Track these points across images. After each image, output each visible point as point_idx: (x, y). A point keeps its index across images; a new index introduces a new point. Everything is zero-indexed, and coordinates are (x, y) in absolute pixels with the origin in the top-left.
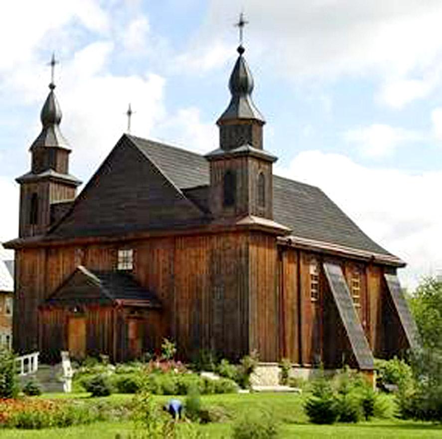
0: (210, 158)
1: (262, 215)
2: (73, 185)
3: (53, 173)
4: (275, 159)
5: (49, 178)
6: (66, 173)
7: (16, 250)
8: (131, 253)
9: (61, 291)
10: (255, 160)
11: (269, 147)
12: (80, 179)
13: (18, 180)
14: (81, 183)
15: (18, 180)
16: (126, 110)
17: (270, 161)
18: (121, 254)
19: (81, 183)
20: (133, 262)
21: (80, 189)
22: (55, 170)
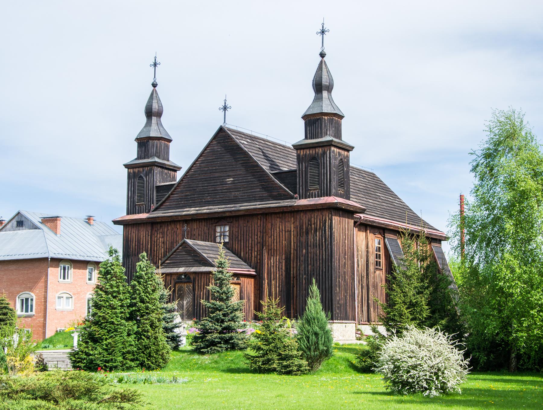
0: (297, 147)
1: (341, 196)
2: (175, 169)
3: (157, 160)
4: (181, 168)
5: (154, 164)
6: (168, 160)
7: (124, 225)
8: (227, 228)
9: (172, 256)
10: (376, 230)
11: (346, 138)
12: (178, 164)
13: (126, 166)
14: (180, 168)
15: (126, 166)
16: (222, 105)
17: (348, 149)
18: (218, 229)
19: (180, 168)
20: (229, 236)
21: (179, 175)
22: (159, 157)
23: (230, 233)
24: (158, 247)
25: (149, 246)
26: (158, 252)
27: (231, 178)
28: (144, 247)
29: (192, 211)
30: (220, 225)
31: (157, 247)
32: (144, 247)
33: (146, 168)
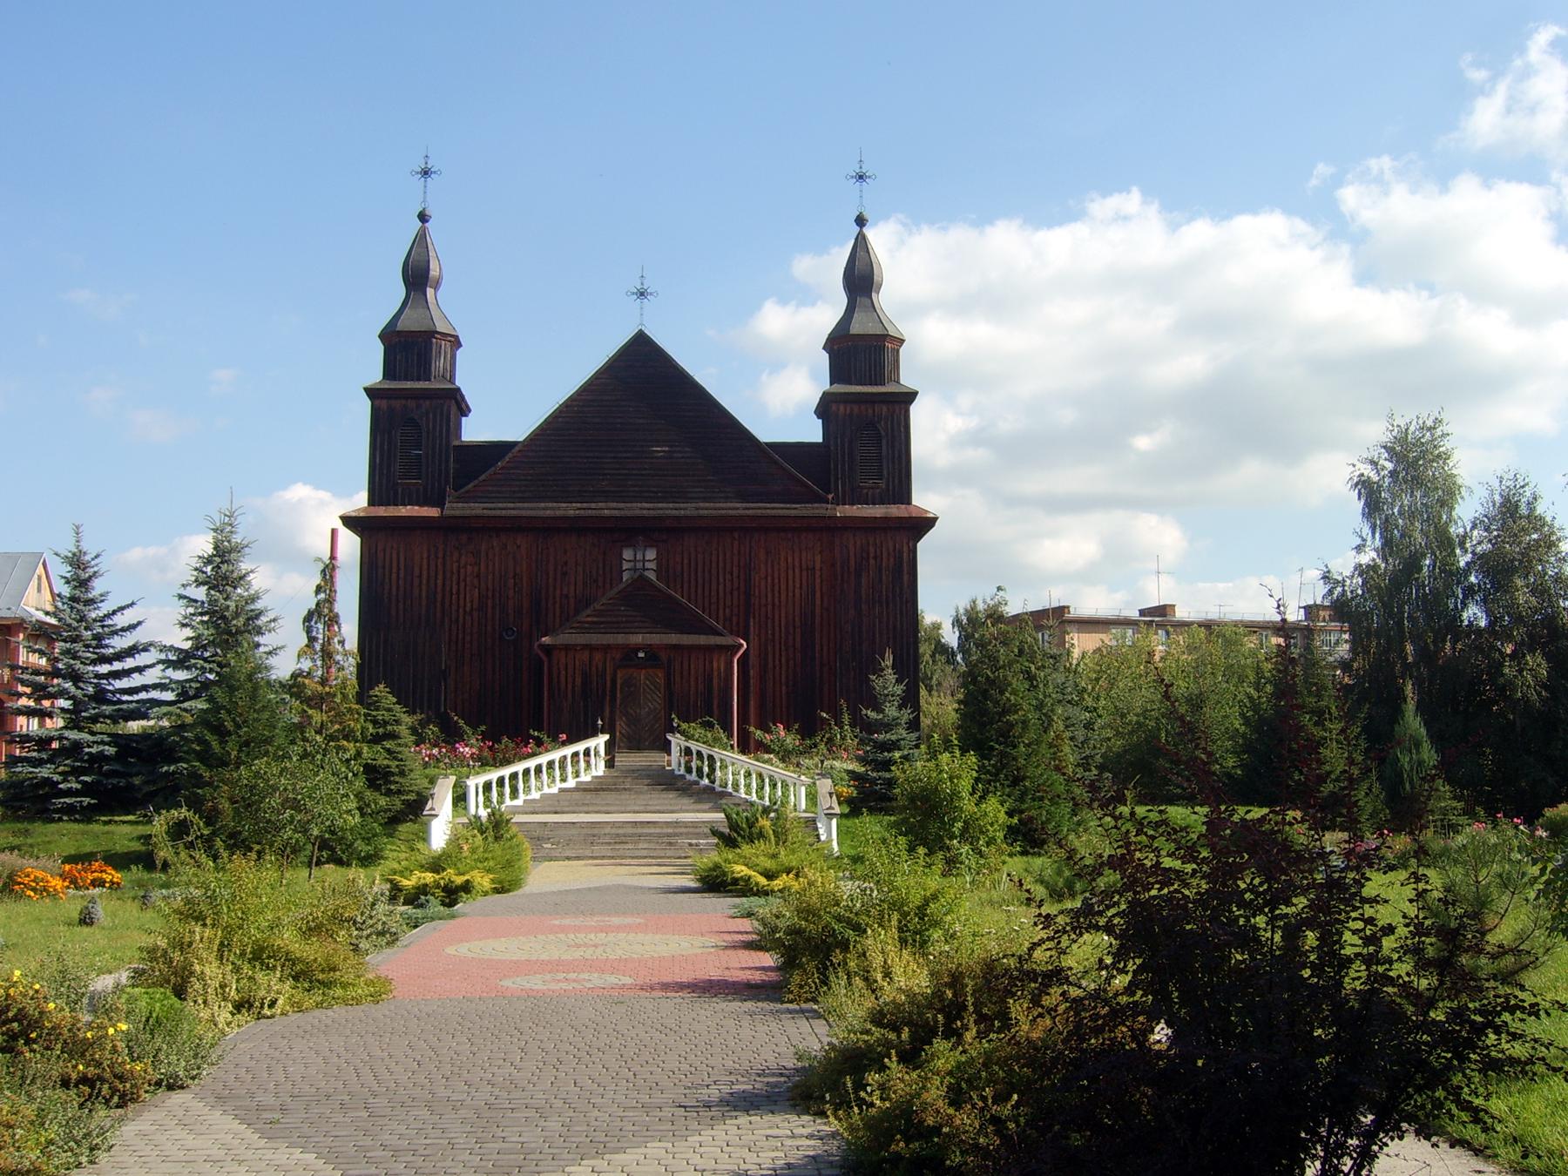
8: (651, 554)
18: (627, 554)
23: (659, 565)
24: (462, 584)
25: (440, 582)
26: (462, 596)
27: (666, 446)
28: (424, 582)
29: (570, 509)
30: (633, 546)
31: (458, 583)
32: (424, 582)
33: (428, 402)
